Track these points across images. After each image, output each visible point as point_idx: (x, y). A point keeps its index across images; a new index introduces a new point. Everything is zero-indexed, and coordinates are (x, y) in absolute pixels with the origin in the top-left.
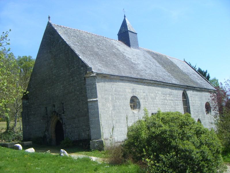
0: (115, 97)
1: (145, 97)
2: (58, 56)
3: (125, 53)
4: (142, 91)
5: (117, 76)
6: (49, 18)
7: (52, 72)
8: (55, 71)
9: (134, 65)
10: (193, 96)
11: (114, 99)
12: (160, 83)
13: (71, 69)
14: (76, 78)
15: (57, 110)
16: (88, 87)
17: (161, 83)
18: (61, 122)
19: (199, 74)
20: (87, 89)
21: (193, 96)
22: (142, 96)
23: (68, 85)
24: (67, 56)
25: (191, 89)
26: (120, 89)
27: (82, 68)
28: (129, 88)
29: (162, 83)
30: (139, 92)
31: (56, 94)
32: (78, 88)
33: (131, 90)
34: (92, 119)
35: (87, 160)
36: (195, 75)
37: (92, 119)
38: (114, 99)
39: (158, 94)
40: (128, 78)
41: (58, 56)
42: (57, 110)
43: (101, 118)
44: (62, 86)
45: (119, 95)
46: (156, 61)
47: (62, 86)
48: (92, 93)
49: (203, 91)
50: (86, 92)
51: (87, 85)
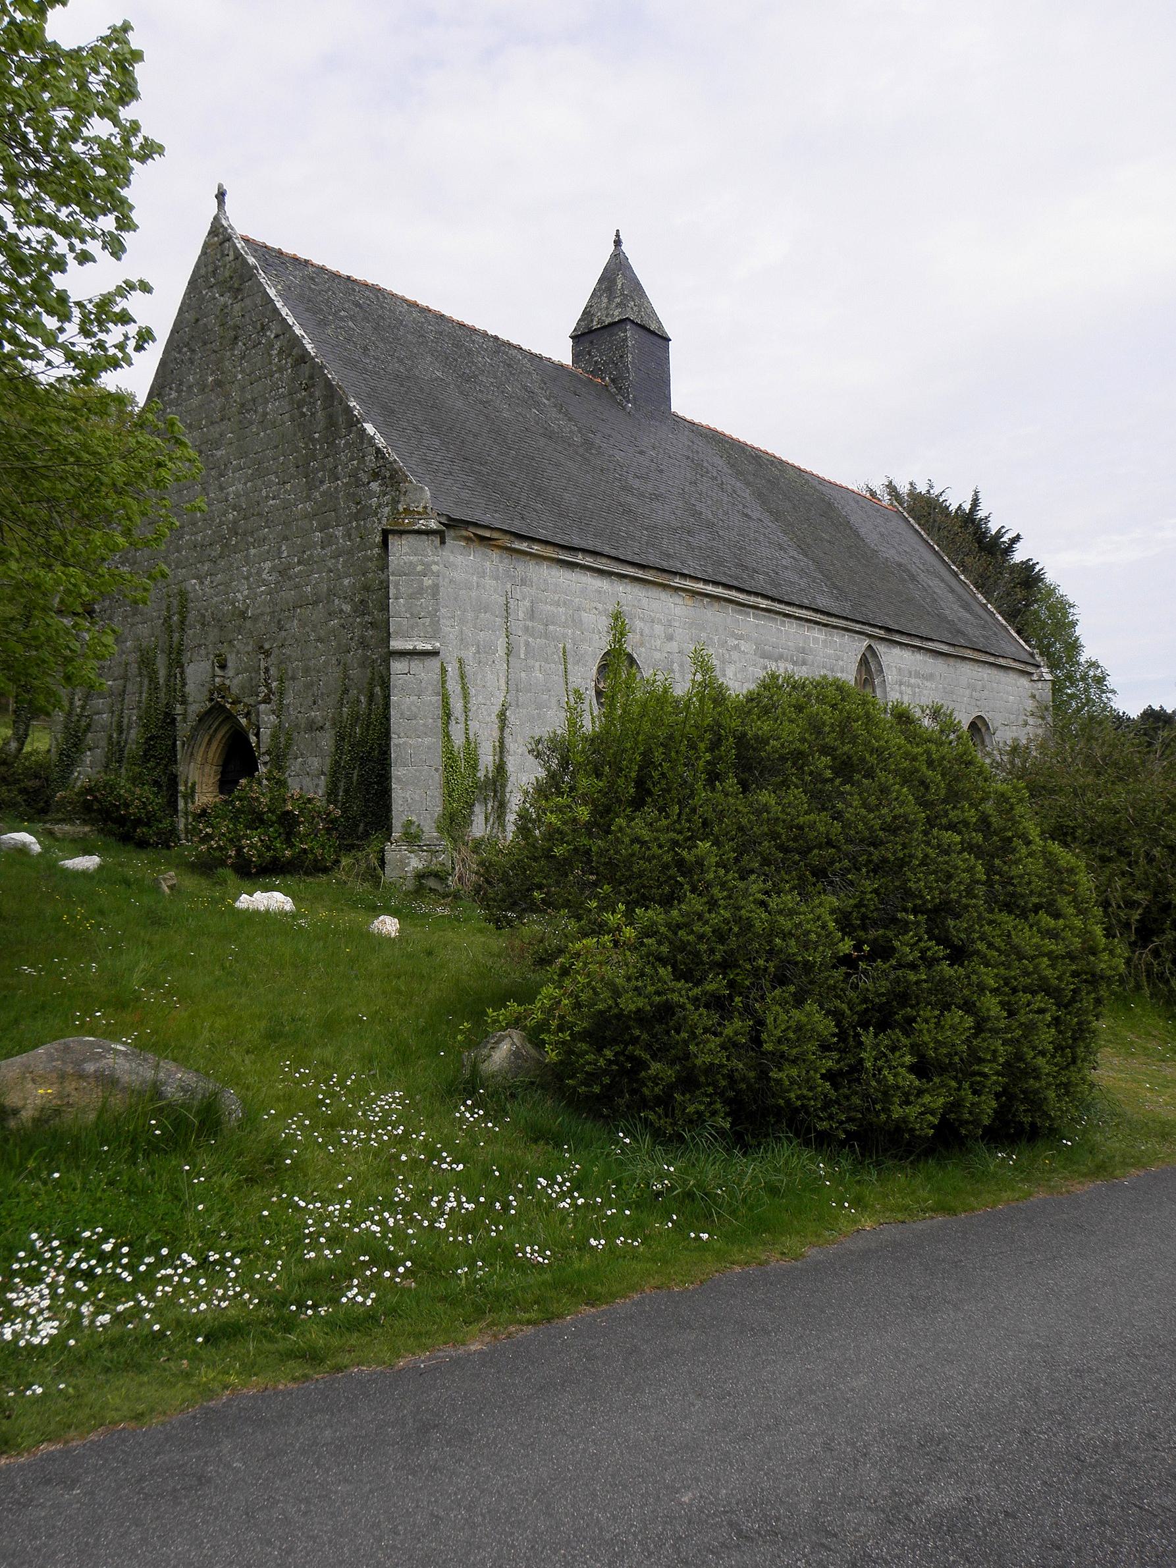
0: (527, 644)
1: (673, 662)
2: (255, 411)
3: (599, 435)
4: (658, 629)
5: (387, 705)
6: (221, 196)
7: (222, 488)
8: (240, 486)
9: (634, 500)
10: (913, 681)
11: (522, 656)
12: (752, 598)
13: (322, 482)
14: (339, 532)
15: (236, 681)
16: (397, 584)
17: (759, 600)
18: (253, 739)
19: (956, 575)
20: (392, 591)
21: (913, 681)
22: (657, 655)
23: (299, 563)
24: (304, 415)
25: (907, 645)
26: (553, 608)
27: (374, 486)
28: (600, 606)
29: (766, 602)
30: (647, 631)
31: (233, 604)
32: (346, 582)
33: (608, 616)
34: (401, 741)
35: (633, 363)
36: (937, 582)
37: (401, 741)
38: (522, 656)
39: (740, 652)
40: (599, 559)
41: (260, 410)
42: (236, 681)
43: (466, 696)
44: (268, 564)
45: (546, 635)
46: (747, 493)
47: (268, 564)
48: (412, 614)
49: (966, 658)
50: (385, 608)
51: (393, 574)
